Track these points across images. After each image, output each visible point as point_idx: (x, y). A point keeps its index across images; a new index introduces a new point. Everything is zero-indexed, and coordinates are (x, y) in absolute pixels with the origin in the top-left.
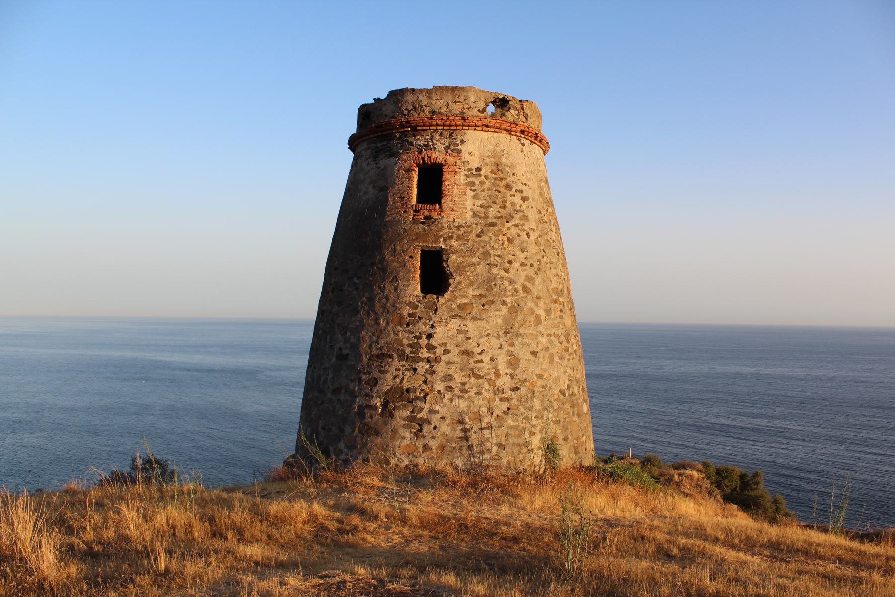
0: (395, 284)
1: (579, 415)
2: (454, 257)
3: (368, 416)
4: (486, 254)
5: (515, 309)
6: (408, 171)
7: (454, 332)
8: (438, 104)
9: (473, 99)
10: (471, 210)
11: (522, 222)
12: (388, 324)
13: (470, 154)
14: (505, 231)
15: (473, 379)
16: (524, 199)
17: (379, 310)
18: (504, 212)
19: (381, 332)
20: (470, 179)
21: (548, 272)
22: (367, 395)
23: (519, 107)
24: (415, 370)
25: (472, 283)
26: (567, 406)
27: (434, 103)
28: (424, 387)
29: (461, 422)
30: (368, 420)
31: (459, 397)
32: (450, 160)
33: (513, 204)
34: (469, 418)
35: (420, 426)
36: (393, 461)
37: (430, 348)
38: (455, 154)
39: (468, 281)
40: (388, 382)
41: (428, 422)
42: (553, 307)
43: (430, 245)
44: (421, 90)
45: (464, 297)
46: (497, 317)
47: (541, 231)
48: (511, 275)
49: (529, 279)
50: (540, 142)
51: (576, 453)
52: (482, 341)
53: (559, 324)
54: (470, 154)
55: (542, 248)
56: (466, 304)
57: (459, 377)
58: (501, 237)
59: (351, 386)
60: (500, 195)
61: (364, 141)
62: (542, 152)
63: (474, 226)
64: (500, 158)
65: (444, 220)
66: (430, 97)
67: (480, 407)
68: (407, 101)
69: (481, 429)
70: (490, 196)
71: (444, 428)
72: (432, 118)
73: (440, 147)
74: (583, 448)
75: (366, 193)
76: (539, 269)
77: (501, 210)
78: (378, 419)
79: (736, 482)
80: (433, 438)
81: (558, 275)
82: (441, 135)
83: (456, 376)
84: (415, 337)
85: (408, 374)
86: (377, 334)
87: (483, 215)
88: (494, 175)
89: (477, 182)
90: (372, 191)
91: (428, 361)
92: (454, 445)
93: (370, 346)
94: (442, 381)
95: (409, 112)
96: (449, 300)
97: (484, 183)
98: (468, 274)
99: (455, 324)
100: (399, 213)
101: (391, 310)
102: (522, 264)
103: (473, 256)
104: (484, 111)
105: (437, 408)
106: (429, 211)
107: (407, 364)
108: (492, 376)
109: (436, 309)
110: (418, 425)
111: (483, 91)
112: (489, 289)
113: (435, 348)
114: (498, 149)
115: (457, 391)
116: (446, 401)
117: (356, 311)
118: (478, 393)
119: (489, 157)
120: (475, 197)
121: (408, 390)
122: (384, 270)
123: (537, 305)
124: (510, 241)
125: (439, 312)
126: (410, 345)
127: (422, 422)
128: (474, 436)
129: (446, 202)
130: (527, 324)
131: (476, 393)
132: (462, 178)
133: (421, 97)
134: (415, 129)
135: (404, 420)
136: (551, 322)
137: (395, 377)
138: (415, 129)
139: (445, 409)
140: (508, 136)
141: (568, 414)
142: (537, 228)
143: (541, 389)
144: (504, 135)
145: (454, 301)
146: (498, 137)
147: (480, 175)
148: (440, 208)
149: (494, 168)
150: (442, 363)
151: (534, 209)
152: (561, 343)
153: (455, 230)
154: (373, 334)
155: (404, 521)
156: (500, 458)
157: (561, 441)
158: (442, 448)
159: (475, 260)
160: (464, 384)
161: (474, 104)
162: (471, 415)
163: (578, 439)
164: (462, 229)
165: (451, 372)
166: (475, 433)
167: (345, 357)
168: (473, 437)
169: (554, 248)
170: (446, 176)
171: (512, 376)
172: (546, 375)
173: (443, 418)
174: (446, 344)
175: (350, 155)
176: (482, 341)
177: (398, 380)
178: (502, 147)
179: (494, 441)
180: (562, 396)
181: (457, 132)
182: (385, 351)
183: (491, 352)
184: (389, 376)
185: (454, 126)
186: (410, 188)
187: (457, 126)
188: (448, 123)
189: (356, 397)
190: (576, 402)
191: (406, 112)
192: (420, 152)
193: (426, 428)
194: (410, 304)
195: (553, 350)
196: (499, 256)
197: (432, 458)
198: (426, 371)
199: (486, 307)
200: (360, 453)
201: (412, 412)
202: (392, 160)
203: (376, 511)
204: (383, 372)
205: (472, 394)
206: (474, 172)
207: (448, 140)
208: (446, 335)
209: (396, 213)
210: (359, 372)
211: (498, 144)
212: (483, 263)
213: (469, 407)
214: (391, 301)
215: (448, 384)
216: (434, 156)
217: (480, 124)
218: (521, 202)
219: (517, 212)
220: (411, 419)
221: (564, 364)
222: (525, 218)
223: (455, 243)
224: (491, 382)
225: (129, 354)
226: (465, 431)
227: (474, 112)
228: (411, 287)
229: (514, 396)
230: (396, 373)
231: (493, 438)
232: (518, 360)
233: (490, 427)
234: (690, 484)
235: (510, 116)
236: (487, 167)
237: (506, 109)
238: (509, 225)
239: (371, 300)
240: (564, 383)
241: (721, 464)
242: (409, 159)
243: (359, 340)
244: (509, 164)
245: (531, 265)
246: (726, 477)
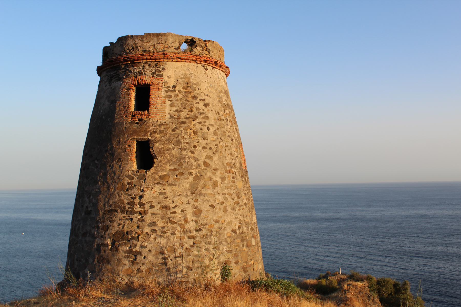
0: (120, 164)
1: (247, 246)
3: (102, 251)
4: (179, 142)
5: (198, 178)
6: (129, 89)
7: (157, 194)
8: (148, 45)
10: (169, 113)
11: (204, 120)
12: (115, 190)
13: (168, 77)
14: (192, 126)
15: (169, 224)
16: (206, 105)
17: (110, 181)
18: (191, 114)
19: (110, 195)
20: (168, 94)
21: (223, 152)
22: (102, 237)
23: (203, 45)
24: (132, 219)
25: (169, 161)
26: (238, 241)
27: (145, 44)
28: (137, 230)
29: (162, 253)
30: (102, 253)
31: (160, 236)
32: (155, 81)
33: (197, 109)
34: (167, 250)
35: (135, 256)
36: (118, 280)
37: (141, 205)
38: (159, 77)
39: (166, 160)
41: (140, 253)
43: (142, 137)
44: (137, 37)
45: (163, 170)
46: (186, 183)
47: (219, 126)
48: (196, 155)
50: (220, 67)
51: (245, 272)
52: (176, 199)
53: (232, 186)
54: (168, 77)
55: (219, 137)
56: (164, 175)
57: (160, 223)
59: (93, 232)
60: (189, 103)
61: (104, 70)
62: (223, 74)
63: (171, 124)
64: (189, 78)
65: (151, 121)
66: (142, 41)
67: (175, 242)
69: (176, 257)
70: (182, 104)
71: (151, 257)
72: (143, 55)
73: (149, 73)
74: (252, 268)
75: (104, 105)
76: (216, 151)
77: (189, 113)
78: (109, 252)
80: (143, 264)
81: (231, 154)
82: (150, 65)
84: (132, 198)
85: (127, 222)
86: (108, 197)
87: (176, 117)
88: (185, 90)
89: (173, 95)
90: (107, 103)
92: (157, 268)
93: (104, 205)
94: (149, 226)
95: (130, 51)
96: (154, 173)
98: (166, 155)
99: (157, 189)
100: (122, 117)
101: (117, 181)
102: (204, 148)
103: (169, 143)
104: (178, 48)
106: (142, 115)
107: (127, 216)
109: (145, 179)
110: (134, 256)
111: (177, 35)
113: (144, 204)
114: (188, 73)
115: (159, 233)
117: (96, 182)
118: (173, 234)
119: (181, 78)
120: (172, 105)
121: (127, 233)
122: (113, 154)
123: (214, 174)
124: (195, 133)
125: (147, 181)
126: (128, 203)
127: (137, 254)
128: (171, 262)
129: (152, 109)
130: (207, 187)
132: (163, 93)
133: (137, 41)
134: (133, 62)
135: (125, 253)
136: (225, 185)
137: (119, 224)
138: (133, 62)
139: (151, 245)
140: (196, 64)
141: (239, 246)
142: (216, 124)
144: (192, 64)
145: (157, 174)
146: (188, 65)
148: (148, 113)
149: (185, 85)
150: (149, 215)
151: (214, 112)
152: (233, 199)
153: (158, 127)
154: (106, 197)
156: (188, 277)
157: (233, 264)
158: (149, 270)
159: (171, 146)
160: (163, 228)
162: (169, 248)
163: (247, 262)
164: (163, 126)
165: (155, 220)
166: (171, 260)
168: (170, 262)
169: (229, 136)
170: (152, 92)
171: (196, 222)
172: (221, 220)
173: (150, 251)
174: (151, 202)
176: (176, 199)
177: (121, 226)
178: (191, 71)
179: (184, 265)
180: (234, 234)
181: (160, 63)
182: (113, 208)
183: (181, 206)
184: (116, 224)
185: (158, 59)
186: (129, 100)
187: (160, 59)
188: (154, 57)
189: (95, 238)
191: (128, 51)
192: (136, 77)
193: (139, 257)
194: (129, 177)
196: (187, 143)
197: (143, 278)
198: (139, 219)
199: (178, 176)
200: (98, 276)
201: (130, 247)
202: (119, 82)
204: (112, 221)
205: (169, 234)
206: (171, 89)
207: (154, 69)
208: (151, 196)
209: (121, 117)
210: (97, 222)
211: (188, 70)
212: (176, 148)
213: (167, 243)
214: (117, 175)
215: (153, 228)
216: (144, 79)
217: (175, 57)
218: (204, 107)
219: (200, 114)
220: (130, 252)
221: (235, 213)
222: (207, 118)
223: (157, 136)
224: (182, 226)
225: (15, 215)
226: (165, 259)
229: (198, 235)
231: (183, 263)
232: (200, 211)
233: (181, 256)
234: (355, 291)
235: (196, 51)
236: (180, 85)
237: (194, 46)
238: (195, 122)
239: (105, 174)
240: (236, 225)
241: (380, 277)
242: (129, 81)
245: (211, 148)
246: (384, 286)
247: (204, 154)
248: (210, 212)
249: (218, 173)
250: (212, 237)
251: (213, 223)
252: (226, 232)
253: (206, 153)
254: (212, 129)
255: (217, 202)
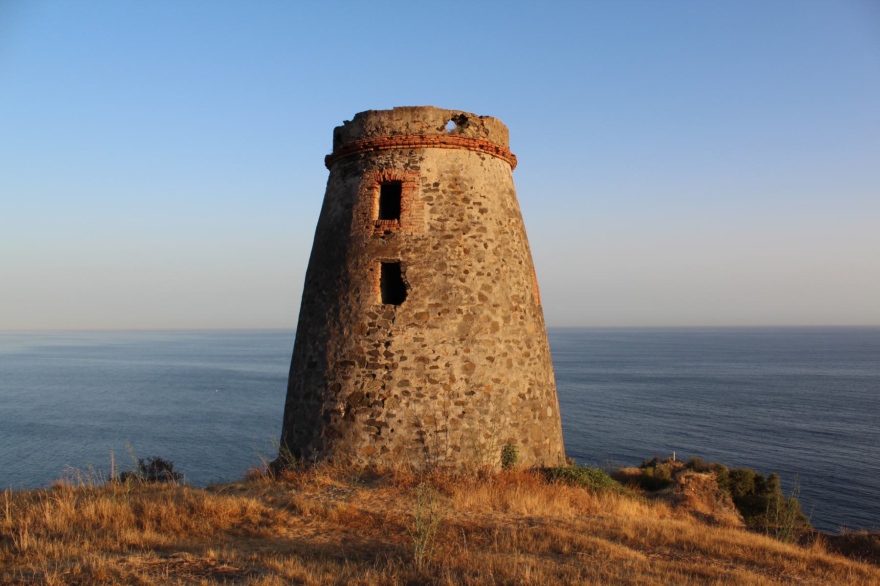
1: (540, 418)
2: (411, 268)
3: (333, 420)
4: (442, 265)
6: (371, 188)
7: (410, 340)
8: (399, 124)
9: (431, 118)
11: (479, 233)
12: (350, 333)
13: (428, 170)
14: (461, 242)
15: (428, 384)
17: (343, 320)
19: (344, 341)
22: (332, 400)
23: (478, 123)
24: (374, 376)
25: (428, 293)
26: (527, 410)
27: (394, 123)
28: (382, 392)
29: (417, 425)
30: (332, 423)
31: (415, 401)
32: (409, 177)
33: (470, 217)
35: (379, 428)
37: (388, 355)
40: (350, 388)
41: (386, 425)
42: (512, 314)
43: (389, 258)
44: (383, 112)
45: (420, 306)
46: (452, 325)
48: (467, 284)
49: (486, 287)
50: (503, 155)
53: (519, 330)
54: (428, 170)
55: (501, 257)
56: (422, 313)
57: (414, 383)
58: (457, 249)
59: (319, 392)
60: (457, 208)
62: (508, 166)
64: (458, 172)
65: (403, 234)
66: (391, 118)
67: (435, 411)
68: (370, 123)
69: (437, 432)
70: (447, 210)
72: (391, 138)
73: (399, 165)
74: (546, 450)
75: (335, 210)
76: (497, 278)
79: (750, 485)
80: (390, 440)
81: (518, 283)
82: (401, 153)
83: (412, 381)
84: (375, 345)
85: (368, 380)
89: (435, 197)
91: (387, 368)
92: (410, 447)
93: (335, 354)
94: (399, 386)
96: (407, 310)
97: (442, 197)
98: (424, 284)
99: (411, 332)
100: (361, 229)
101: (354, 320)
102: (479, 274)
103: (429, 267)
104: (443, 128)
105: (394, 412)
108: (447, 381)
110: (377, 428)
111: (441, 110)
112: (445, 298)
113: (392, 355)
114: (457, 165)
115: (413, 396)
116: (402, 405)
117: (324, 322)
118: (434, 398)
119: (447, 172)
120: (433, 211)
121: (368, 395)
122: (347, 282)
123: (494, 312)
124: (466, 252)
125: (396, 321)
126: (369, 353)
128: (429, 438)
129: (405, 217)
130: (483, 330)
131: (431, 398)
132: (420, 194)
133: (383, 119)
134: (377, 149)
135: (364, 423)
136: (509, 328)
137: (357, 383)
138: (377, 149)
139: (402, 413)
141: (528, 417)
142: (496, 238)
143: (499, 393)
144: (463, 151)
145: (410, 310)
147: (438, 190)
148: (399, 222)
149: (452, 182)
150: (399, 369)
151: (494, 221)
152: (521, 349)
153: (412, 243)
154: (338, 343)
155: (325, 516)
157: (519, 444)
158: (399, 450)
159: (431, 271)
160: (420, 389)
161: (433, 121)
162: (427, 419)
164: (419, 242)
165: (407, 378)
166: (431, 435)
167: (312, 365)
168: (428, 438)
169: (515, 257)
170: (404, 192)
171: (467, 381)
172: (503, 380)
173: (400, 421)
174: (402, 351)
175: (328, 172)
177: (359, 386)
178: (460, 162)
179: (449, 443)
180: (521, 400)
182: (348, 358)
183: (446, 358)
184: (351, 382)
185: (413, 145)
186: (371, 204)
187: (415, 144)
189: (323, 402)
190: (538, 406)
191: (370, 133)
192: (381, 171)
193: (384, 431)
195: (510, 356)
196: (455, 267)
197: (389, 459)
198: (385, 376)
199: (442, 315)
200: (326, 455)
201: (372, 416)
202: (357, 178)
203: (302, 507)
204: (346, 378)
205: (427, 398)
208: (403, 343)
209: (359, 229)
210: (326, 378)
212: (439, 273)
213: (424, 411)
214: (353, 311)
217: (437, 141)
218: (479, 214)
219: (475, 223)
220: (371, 422)
221: (523, 369)
222: (484, 229)
223: (412, 255)
226: (421, 433)
227: (433, 130)
228: (371, 298)
230: (357, 379)
231: (448, 441)
233: (445, 430)
234: (697, 487)
235: (469, 133)
236: (445, 182)
238: (466, 236)
239: (337, 311)
240: (524, 387)
242: (371, 177)
243: (325, 348)
244: (467, 178)
245: (489, 275)
246: (740, 479)
247: (479, 283)
248: (488, 367)
249: (499, 311)
250: (490, 404)
251: (491, 383)
252: (510, 397)
253: (482, 282)
254: (491, 247)
255: (497, 353)
